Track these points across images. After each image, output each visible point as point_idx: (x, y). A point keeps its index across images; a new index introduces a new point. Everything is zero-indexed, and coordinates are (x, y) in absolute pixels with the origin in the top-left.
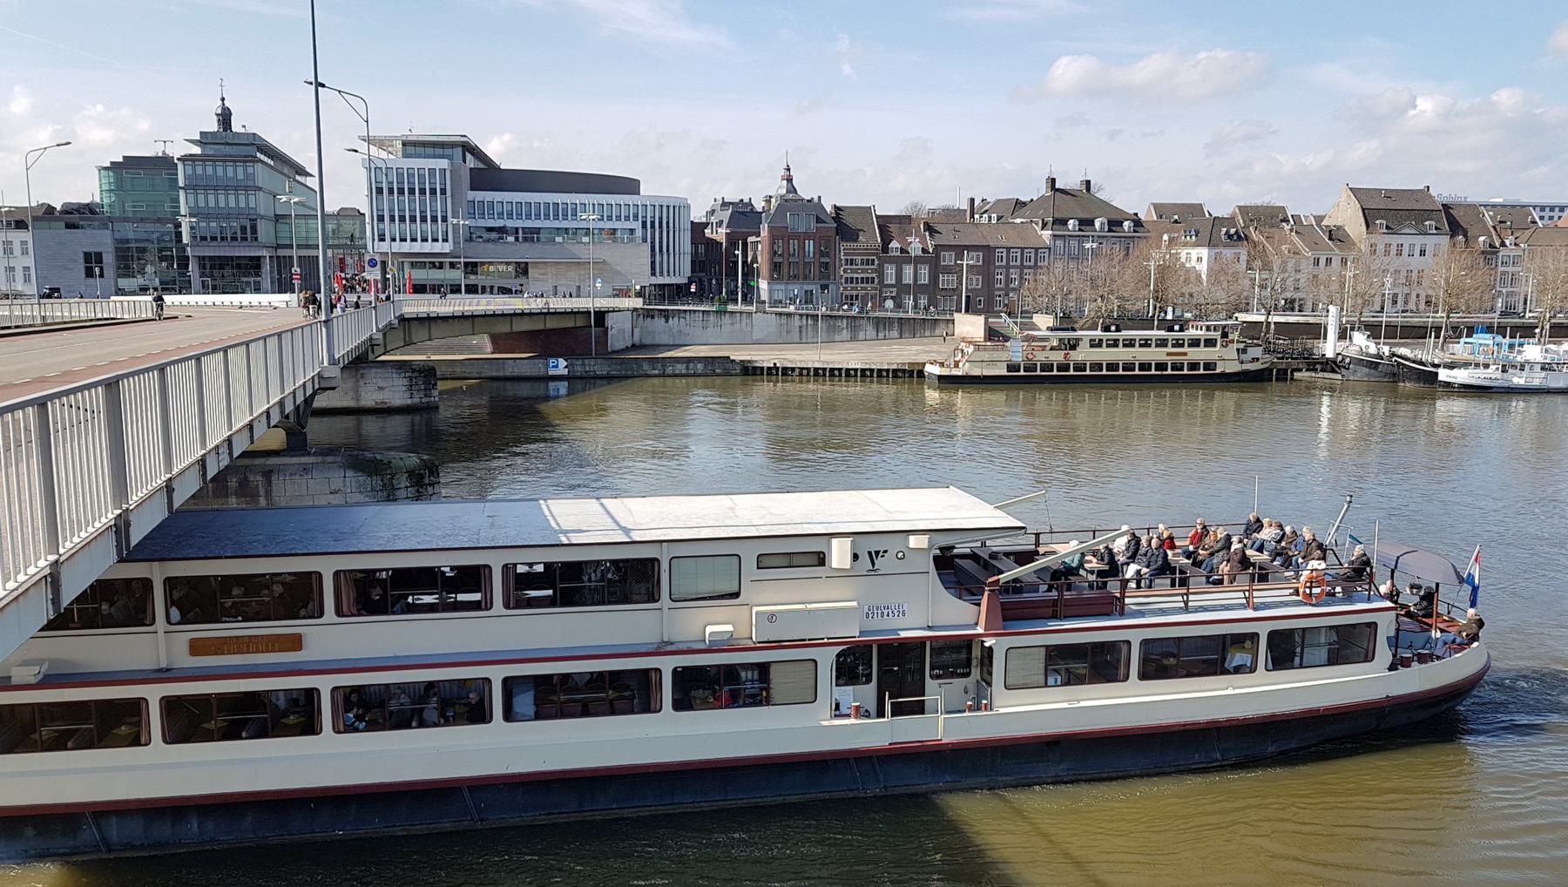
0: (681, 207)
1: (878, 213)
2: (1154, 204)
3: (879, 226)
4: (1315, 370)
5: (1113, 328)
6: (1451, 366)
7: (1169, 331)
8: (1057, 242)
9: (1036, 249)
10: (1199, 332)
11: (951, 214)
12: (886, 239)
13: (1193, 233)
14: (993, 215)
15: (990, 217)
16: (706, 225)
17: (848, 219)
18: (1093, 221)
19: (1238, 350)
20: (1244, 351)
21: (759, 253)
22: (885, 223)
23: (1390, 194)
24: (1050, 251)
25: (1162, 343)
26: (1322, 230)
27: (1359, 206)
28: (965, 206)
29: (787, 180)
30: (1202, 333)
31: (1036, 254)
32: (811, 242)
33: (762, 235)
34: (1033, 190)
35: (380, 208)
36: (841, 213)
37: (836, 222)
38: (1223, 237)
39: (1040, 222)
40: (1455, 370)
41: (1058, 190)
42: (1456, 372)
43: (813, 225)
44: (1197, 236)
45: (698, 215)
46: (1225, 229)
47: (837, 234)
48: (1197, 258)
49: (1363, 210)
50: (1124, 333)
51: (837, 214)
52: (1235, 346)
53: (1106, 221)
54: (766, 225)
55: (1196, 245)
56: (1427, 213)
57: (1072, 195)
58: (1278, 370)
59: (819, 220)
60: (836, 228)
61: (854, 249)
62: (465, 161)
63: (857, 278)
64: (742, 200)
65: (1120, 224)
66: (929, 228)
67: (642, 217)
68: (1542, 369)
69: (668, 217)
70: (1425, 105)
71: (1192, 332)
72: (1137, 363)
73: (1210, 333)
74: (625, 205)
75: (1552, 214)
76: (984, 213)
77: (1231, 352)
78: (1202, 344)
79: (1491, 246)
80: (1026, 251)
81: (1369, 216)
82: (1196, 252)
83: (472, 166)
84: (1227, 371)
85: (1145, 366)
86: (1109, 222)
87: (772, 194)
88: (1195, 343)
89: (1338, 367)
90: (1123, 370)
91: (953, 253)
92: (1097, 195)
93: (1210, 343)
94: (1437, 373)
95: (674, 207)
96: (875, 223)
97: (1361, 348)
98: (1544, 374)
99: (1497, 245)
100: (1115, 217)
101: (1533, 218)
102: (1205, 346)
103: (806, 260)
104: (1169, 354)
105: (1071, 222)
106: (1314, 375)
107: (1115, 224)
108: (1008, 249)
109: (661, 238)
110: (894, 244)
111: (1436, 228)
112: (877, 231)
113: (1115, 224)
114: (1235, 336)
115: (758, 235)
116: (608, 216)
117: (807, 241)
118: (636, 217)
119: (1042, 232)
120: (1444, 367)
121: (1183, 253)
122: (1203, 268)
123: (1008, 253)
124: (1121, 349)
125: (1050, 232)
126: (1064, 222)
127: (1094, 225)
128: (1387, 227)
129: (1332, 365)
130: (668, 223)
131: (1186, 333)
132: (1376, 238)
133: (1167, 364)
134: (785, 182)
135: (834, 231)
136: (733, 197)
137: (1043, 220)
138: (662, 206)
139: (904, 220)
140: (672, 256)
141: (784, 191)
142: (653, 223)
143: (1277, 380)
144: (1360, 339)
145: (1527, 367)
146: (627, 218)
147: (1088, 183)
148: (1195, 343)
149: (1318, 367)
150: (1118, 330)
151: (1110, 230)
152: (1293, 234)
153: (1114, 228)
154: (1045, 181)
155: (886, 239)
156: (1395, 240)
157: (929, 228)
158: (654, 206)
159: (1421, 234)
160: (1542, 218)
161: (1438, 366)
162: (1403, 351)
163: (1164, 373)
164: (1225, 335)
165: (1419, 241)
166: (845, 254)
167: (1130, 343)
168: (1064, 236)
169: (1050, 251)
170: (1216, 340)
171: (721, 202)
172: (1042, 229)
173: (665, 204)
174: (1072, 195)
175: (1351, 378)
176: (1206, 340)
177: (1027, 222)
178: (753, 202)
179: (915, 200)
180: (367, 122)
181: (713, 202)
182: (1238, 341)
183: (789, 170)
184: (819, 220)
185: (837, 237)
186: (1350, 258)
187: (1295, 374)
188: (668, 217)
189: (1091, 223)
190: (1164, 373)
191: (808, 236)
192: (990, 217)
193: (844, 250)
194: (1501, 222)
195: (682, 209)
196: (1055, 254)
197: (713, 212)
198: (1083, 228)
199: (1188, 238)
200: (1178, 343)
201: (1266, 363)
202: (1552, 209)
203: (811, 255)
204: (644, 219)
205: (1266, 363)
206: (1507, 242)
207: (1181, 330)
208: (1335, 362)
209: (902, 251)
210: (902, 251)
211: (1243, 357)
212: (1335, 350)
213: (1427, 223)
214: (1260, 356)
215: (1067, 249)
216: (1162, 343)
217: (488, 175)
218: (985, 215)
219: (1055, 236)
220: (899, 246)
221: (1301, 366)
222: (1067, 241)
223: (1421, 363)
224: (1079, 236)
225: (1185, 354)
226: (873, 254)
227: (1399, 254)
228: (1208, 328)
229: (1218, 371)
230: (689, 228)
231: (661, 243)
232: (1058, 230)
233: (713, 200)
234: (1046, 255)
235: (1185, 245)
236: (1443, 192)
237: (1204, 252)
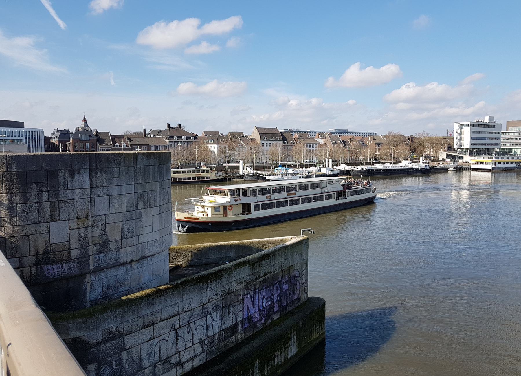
0: (41, 132)
1: (111, 134)
2: (204, 131)
3: (112, 138)
4: (238, 178)
5: (180, 168)
6: (269, 175)
7: (177, 169)
8: (170, 143)
9: (164, 145)
10: (204, 169)
12: (114, 142)
13: (212, 140)
14: (152, 135)
15: (151, 135)
16: (51, 138)
17: (101, 136)
18: (182, 137)
19: (215, 173)
20: (217, 173)
21: (70, 147)
22: (115, 138)
23: (267, 129)
24: (168, 146)
25: (194, 172)
26: (249, 139)
27: (258, 132)
28: (143, 131)
29: (85, 122)
30: (205, 169)
31: (160, 147)
32: (88, 144)
33: (71, 141)
34: (164, 128)
36: (98, 134)
37: (96, 137)
38: (221, 141)
39: (165, 137)
40: (270, 176)
41: (171, 127)
42: (271, 177)
43: (88, 138)
44: (213, 141)
45: (48, 134)
46: (221, 139)
47: (97, 141)
48: (214, 148)
49: (260, 134)
50: (183, 169)
51: (97, 134)
52: (214, 172)
53: (185, 137)
54: (72, 138)
55: (213, 144)
57: (175, 129)
58: (228, 179)
59: (90, 136)
60: (97, 139)
61: (103, 146)
63: (518, 139)
64: (65, 129)
65: (190, 138)
66: (129, 139)
67: (25, 135)
68: (291, 175)
69: (35, 135)
70: (293, 103)
71: (203, 168)
72: (187, 178)
73: (207, 169)
74: (18, 131)
75: (313, 134)
76: (149, 134)
77: (213, 174)
78: (205, 172)
80: (161, 146)
81: (261, 135)
82: (213, 146)
84: (212, 179)
85: (189, 179)
87: (79, 127)
88: (203, 172)
89: (244, 177)
90: (183, 180)
91: (146, 147)
92: (184, 129)
93: (207, 171)
94: (266, 177)
95: (37, 132)
96: (110, 138)
97: (249, 172)
98: (291, 177)
99: (295, 143)
100: (188, 135)
101: (309, 135)
102: (206, 172)
103: (86, 150)
104: (196, 175)
105: (175, 137)
106: (238, 179)
107: (188, 138)
108: (155, 145)
109: (32, 143)
110: (117, 144)
111: (279, 139)
112: (111, 140)
113: (188, 138)
114: (214, 169)
115: (69, 142)
116: (18, 135)
117: (86, 143)
118: (22, 135)
119: (166, 140)
120: (267, 175)
121: (209, 146)
122: (215, 151)
123: (155, 147)
124: (182, 174)
125: (168, 140)
126: (173, 137)
127: (182, 138)
128: (266, 139)
129: (242, 177)
130: (35, 137)
131: (201, 169)
132: (263, 142)
133: (195, 178)
134: (84, 123)
135: (96, 140)
136: (62, 128)
137: (166, 136)
138: (32, 132)
139: (122, 136)
140: (34, 149)
141: (84, 126)
142: (29, 138)
143: (228, 181)
144: (248, 169)
145: (287, 175)
146: (19, 136)
147: (180, 125)
148: (203, 172)
149: (239, 177)
150: (181, 168)
151: (187, 140)
152: (241, 141)
153: (188, 139)
154: (166, 125)
155: (114, 142)
156: (268, 142)
157: (129, 139)
158: (29, 132)
159: (275, 140)
160: (310, 135)
161: (266, 175)
162: (258, 172)
163: (195, 180)
164: (211, 169)
165: (275, 142)
166: (100, 148)
167: (184, 172)
168: (173, 141)
169: (168, 146)
170: (209, 171)
171: (57, 130)
172: (166, 139)
174: (175, 129)
175: (247, 180)
176: (206, 171)
177: (161, 137)
178: (69, 130)
179: (128, 129)
182: (215, 171)
183: (85, 119)
184: (90, 136)
185: (97, 142)
186: (249, 148)
187: (233, 179)
188: (35, 135)
189: (181, 137)
190: (195, 180)
191: (87, 142)
192: (151, 135)
193: (100, 146)
194: (300, 137)
195: (40, 133)
196: (170, 147)
197: (54, 133)
198: (178, 139)
199: (211, 142)
200: (198, 172)
201: (224, 176)
202: (313, 133)
203: (88, 148)
204: (26, 136)
205: (224, 176)
206: (298, 142)
207: (200, 168)
208: (242, 176)
209: (120, 146)
210: (120, 146)
211: (217, 175)
212: (242, 173)
213: (276, 137)
214: (222, 175)
215: (174, 145)
216: (194, 172)
218: (149, 135)
219: (170, 141)
220: (119, 145)
221: (234, 177)
222: (174, 143)
223: (262, 175)
224: (177, 141)
225: (201, 175)
227: (267, 146)
228: (207, 167)
229: (210, 179)
230: (44, 139)
231: (32, 144)
232: (171, 140)
233: (54, 129)
234: (167, 147)
235: (210, 144)
237: (215, 146)
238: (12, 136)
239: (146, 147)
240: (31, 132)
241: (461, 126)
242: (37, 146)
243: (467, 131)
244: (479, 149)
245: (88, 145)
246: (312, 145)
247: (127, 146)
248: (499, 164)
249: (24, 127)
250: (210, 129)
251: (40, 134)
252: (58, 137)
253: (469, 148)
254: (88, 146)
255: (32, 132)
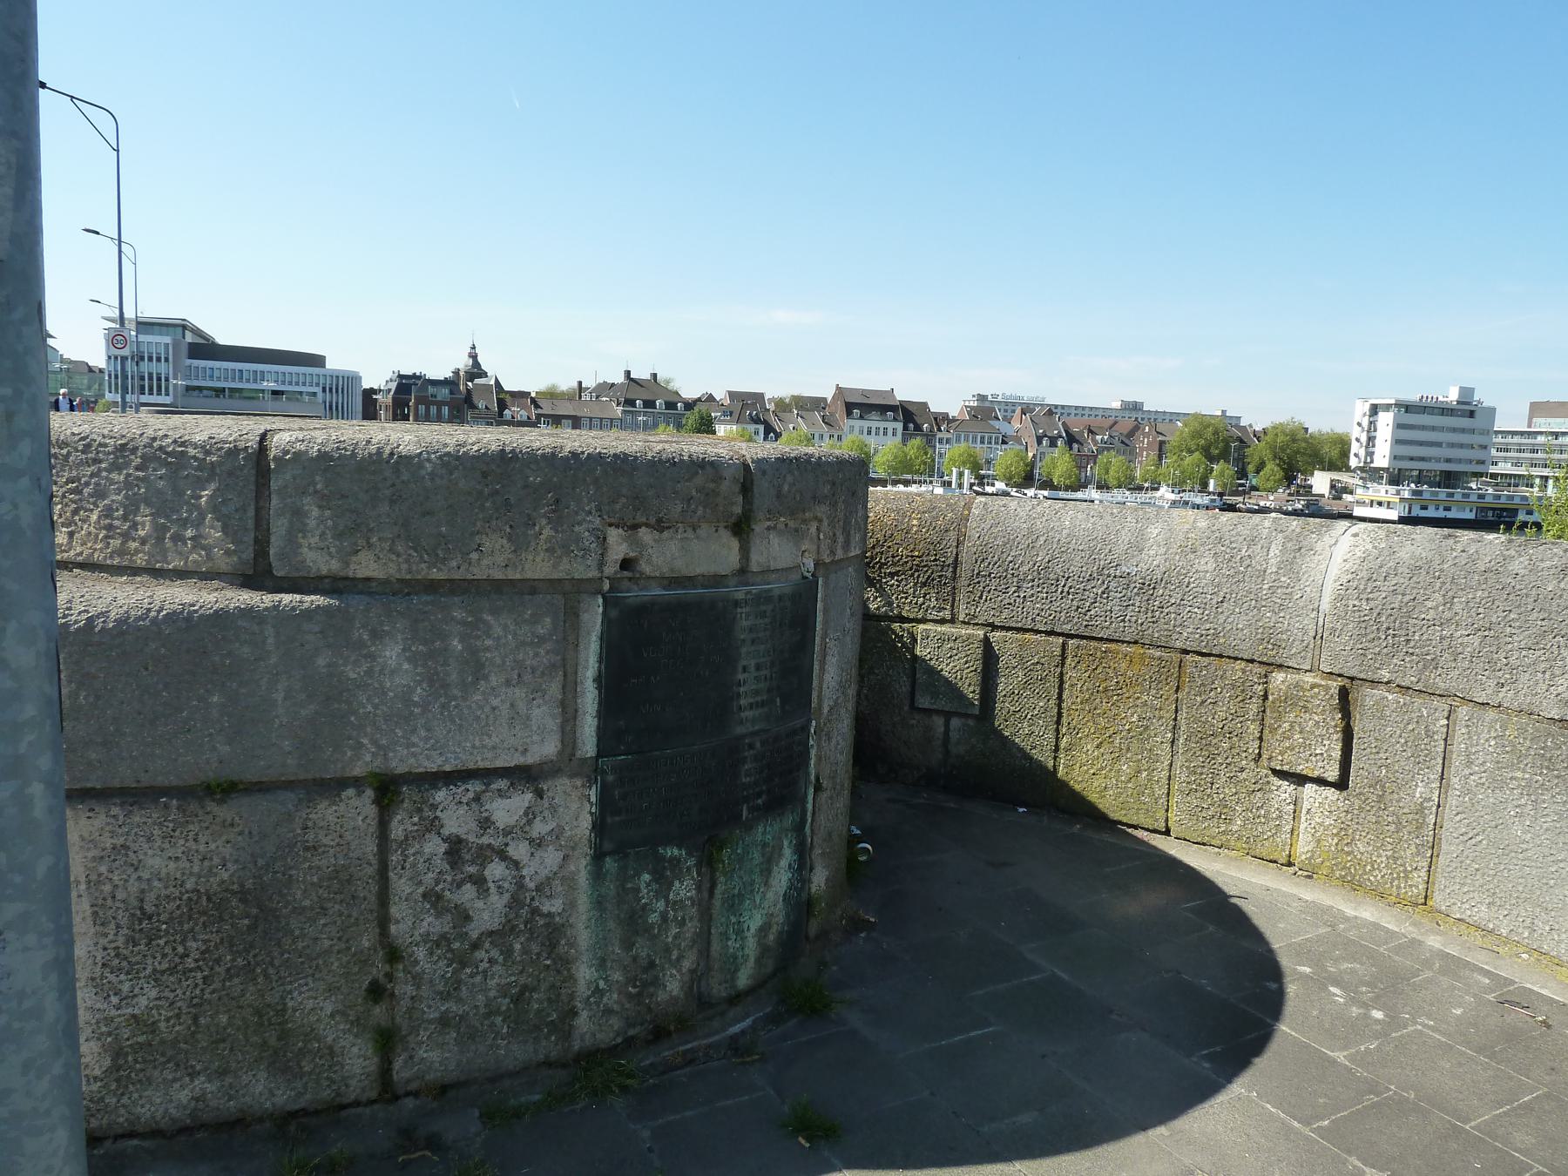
11: (552, 395)
12: (502, 405)
18: (655, 402)
23: (864, 393)
32: (435, 407)
34: (619, 379)
35: (158, 351)
41: (632, 380)
56: (893, 408)
62: (184, 338)
79: (931, 431)
83: (190, 341)
86: (666, 403)
91: (570, 421)
100: (672, 399)
107: (671, 405)
113: (671, 405)
116: (224, 378)
123: (591, 421)
155: (502, 405)
156: (865, 424)
165: (882, 425)
173: (346, 376)
180: (118, 151)
181: (391, 374)
217: (205, 349)
226: (491, 418)
236: (901, 396)
238: (297, 384)
239: (570, 421)
240: (334, 378)
241: (1375, 410)
242: (345, 409)
243: (1386, 420)
244: (1420, 470)
245: (445, 410)
246: (971, 436)
247: (529, 418)
248: (1527, 514)
249: (325, 367)
250: (747, 385)
251: (354, 381)
252: (393, 389)
253: (1387, 466)
254: (447, 413)
255: (337, 377)
